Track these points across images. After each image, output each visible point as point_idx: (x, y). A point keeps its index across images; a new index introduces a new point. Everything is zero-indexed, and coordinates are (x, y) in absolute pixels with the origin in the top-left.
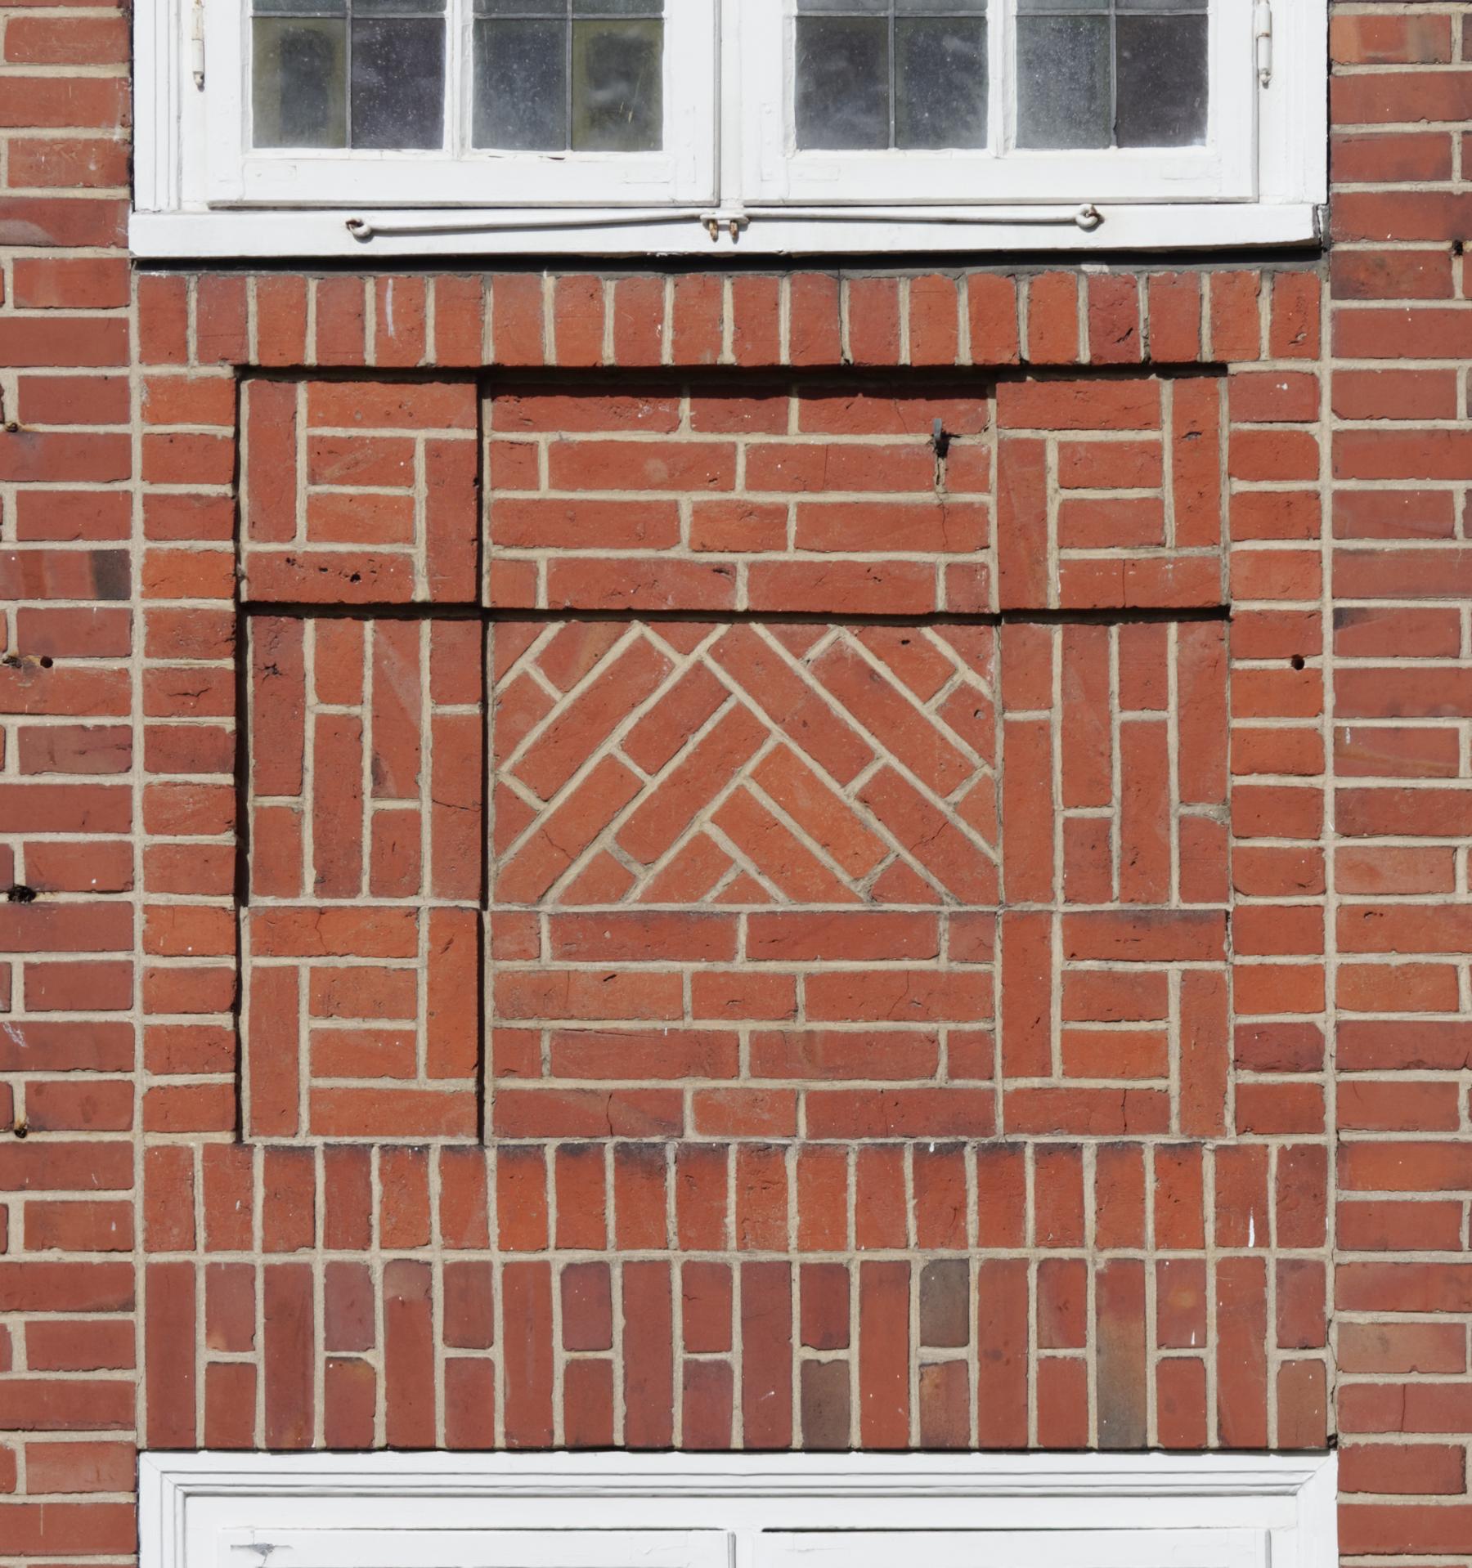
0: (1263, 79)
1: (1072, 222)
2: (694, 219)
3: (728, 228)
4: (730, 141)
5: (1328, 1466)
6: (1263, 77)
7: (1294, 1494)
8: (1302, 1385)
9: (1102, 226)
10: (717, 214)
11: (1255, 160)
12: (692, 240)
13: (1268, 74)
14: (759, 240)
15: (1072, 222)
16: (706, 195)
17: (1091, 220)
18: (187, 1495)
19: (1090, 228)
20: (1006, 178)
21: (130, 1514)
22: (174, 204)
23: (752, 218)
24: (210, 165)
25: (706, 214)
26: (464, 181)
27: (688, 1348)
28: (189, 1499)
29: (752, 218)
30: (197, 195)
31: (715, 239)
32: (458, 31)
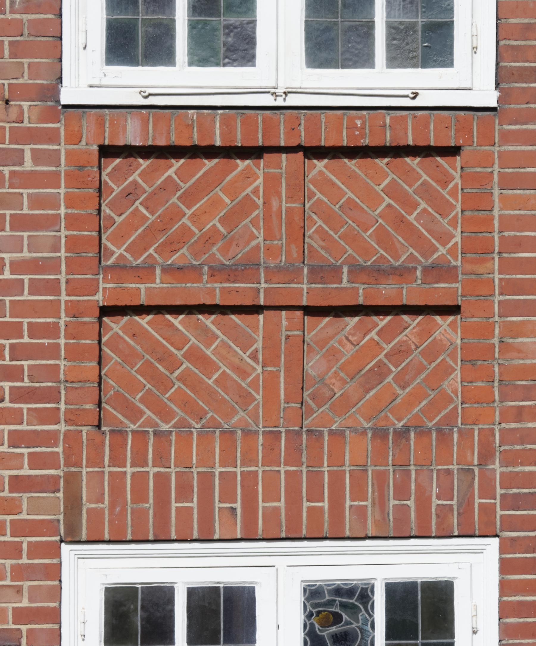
0: (475, 49)
1: (407, 96)
2: (269, 92)
3: (281, 96)
4: (280, 67)
5: (495, 541)
6: (475, 50)
7: (482, 553)
8: (488, 511)
9: (418, 97)
10: (276, 91)
11: (469, 77)
12: (267, 101)
13: (476, 48)
14: (293, 101)
15: (407, 96)
16: (274, 85)
17: (412, 96)
18: (79, 558)
19: (414, 98)
20: (379, 81)
21: (59, 566)
22: (77, 86)
23: (289, 92)
24: (89, 74)
25: (273, 91)
26: (181, 80)
27: (21, 423)
28: (79, 560)
29: (289, 92)
30: (85, 82)
31: (275, 100)
32: (380, 6)
